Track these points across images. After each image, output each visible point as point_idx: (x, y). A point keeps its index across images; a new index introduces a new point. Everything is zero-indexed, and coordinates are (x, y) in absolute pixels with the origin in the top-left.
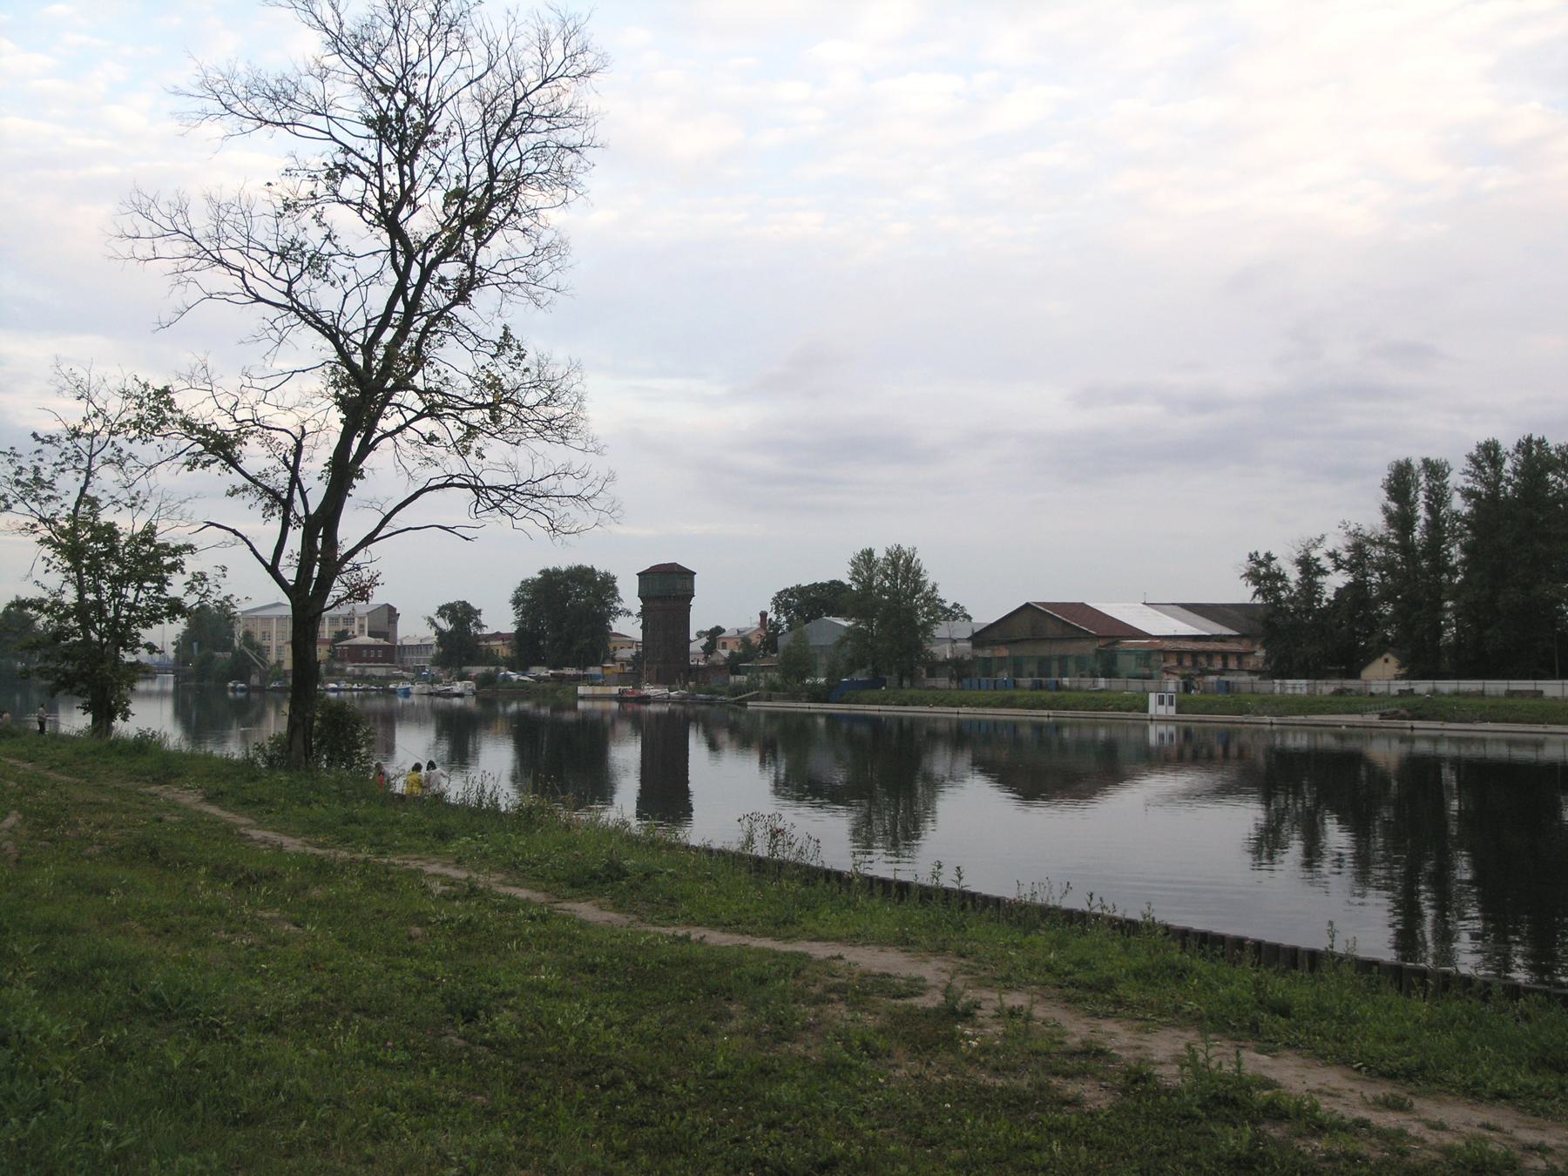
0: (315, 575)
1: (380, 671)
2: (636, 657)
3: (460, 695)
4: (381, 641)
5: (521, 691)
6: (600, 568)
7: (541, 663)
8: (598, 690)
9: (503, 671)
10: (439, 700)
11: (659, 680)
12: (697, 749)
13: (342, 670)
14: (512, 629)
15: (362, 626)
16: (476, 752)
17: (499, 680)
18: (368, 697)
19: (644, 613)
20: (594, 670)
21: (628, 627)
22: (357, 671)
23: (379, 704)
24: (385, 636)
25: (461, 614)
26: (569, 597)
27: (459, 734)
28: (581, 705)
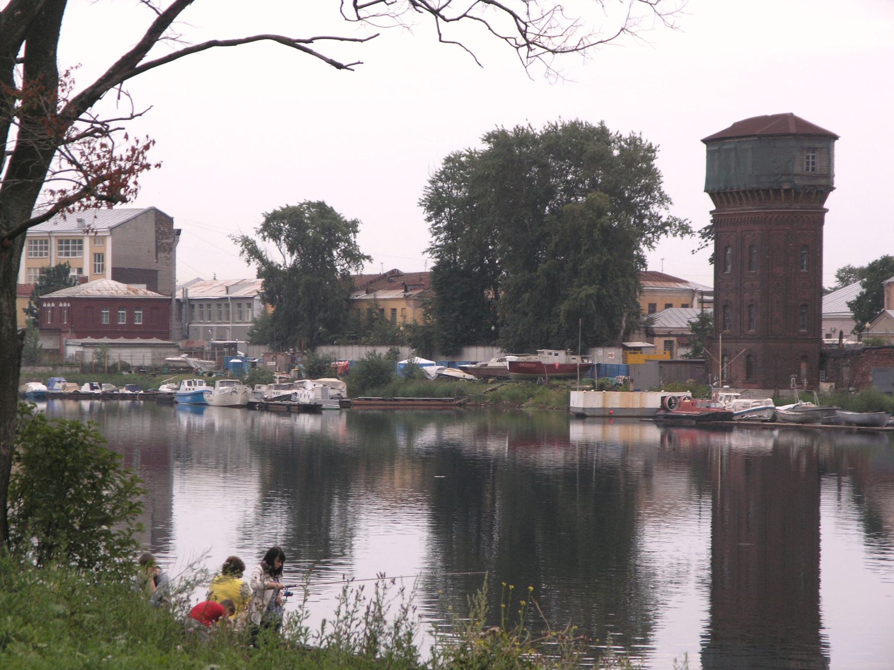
0: (11, 145)
1: (139, 356)
2: (700, 327)
3: (313, 409)
4: (141, 291)
5: (447, 402)
6: (620, 127)
7: (488, 339)
8: (616, 400)
9: (407, 357)
10: (267, 420)
11: (751, 378)
12: (839, 535)
13: (58, 353)
14: (424, 264)
15: (99, 257)
16: (348, 534)
17: (398, 375)
18: (114, 412)
19: (717, 230)
20: (606, 356)
21: (682, 259)
22: (90, 356)
23: (137, 427)
24: (149, 277)
25: (314, 231)
26: (550, 193)
27: (310, 495)
28: (577, 432)
